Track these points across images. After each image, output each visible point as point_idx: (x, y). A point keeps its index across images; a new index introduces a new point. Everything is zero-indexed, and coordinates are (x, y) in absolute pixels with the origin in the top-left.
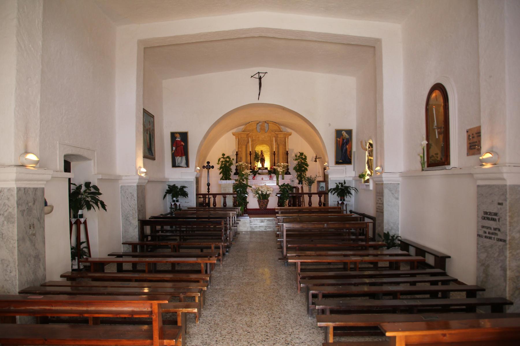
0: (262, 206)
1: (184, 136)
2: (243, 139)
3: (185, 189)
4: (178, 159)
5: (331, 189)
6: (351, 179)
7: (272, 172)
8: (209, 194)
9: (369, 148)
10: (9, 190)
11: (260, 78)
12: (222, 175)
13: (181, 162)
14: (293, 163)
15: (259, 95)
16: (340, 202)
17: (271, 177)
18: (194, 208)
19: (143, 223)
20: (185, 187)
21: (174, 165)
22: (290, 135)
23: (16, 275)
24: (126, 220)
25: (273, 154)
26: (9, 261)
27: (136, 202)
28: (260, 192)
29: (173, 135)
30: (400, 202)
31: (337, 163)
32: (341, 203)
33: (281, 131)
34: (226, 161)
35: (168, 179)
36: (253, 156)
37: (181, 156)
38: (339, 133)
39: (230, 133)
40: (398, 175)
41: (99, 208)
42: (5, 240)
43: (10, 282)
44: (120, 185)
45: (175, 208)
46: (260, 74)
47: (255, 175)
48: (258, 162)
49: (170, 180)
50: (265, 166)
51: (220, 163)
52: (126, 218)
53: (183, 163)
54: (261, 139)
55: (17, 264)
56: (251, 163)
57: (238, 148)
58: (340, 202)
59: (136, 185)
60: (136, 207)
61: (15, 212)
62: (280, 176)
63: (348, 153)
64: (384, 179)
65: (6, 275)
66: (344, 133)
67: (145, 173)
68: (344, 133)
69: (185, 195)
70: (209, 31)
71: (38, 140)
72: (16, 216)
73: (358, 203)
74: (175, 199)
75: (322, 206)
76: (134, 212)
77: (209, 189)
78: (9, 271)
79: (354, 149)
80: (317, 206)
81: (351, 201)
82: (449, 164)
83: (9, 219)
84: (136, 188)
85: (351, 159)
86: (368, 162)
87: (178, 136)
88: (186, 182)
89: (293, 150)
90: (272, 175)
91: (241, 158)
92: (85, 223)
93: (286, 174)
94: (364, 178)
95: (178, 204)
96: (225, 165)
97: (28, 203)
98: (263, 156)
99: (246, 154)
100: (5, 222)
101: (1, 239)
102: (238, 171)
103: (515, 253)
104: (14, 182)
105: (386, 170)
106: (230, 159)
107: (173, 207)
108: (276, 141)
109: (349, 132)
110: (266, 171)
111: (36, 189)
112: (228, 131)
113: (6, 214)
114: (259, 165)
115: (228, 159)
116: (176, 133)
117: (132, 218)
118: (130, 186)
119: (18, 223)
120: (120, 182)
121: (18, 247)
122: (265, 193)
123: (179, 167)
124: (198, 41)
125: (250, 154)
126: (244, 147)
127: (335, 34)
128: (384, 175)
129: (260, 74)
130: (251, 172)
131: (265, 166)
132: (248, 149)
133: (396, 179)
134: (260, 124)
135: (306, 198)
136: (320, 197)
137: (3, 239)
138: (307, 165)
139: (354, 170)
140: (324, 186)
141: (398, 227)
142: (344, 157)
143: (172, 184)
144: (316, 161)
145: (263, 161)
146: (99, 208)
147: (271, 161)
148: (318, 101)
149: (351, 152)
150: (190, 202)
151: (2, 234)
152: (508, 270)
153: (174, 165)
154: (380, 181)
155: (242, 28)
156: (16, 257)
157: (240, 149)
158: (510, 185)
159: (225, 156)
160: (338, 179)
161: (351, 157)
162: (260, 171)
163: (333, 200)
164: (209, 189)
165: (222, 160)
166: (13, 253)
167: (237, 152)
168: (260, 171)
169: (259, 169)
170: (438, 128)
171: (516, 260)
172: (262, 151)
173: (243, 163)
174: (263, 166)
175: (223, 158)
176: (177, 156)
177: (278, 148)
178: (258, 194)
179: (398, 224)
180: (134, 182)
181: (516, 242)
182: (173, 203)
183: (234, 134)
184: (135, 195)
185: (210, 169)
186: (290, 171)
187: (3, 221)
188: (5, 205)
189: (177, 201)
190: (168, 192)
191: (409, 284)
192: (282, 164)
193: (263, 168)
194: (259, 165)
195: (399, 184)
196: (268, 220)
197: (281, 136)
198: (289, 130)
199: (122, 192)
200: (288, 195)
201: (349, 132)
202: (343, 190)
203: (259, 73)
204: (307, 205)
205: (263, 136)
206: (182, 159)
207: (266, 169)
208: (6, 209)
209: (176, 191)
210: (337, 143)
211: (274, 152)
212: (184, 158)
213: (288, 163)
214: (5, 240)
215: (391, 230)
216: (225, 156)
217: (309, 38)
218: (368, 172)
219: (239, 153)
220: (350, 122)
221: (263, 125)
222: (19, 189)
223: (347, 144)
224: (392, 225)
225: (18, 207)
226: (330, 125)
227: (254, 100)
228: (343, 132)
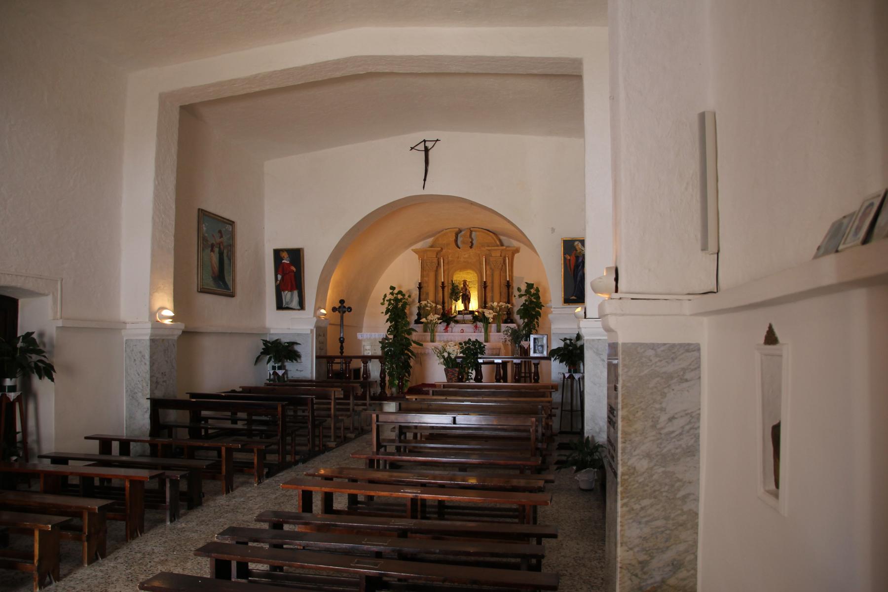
1: (296, 255)
2: (433, 262)
3: (297, 348)
4: (287, 295)
11: (427, 150)
13: (292, 301)
14: (518, 302)
15: (425, 180)
16: (567, 375)
18: (311, 381)
19: (157, 405)
20: (297, 344)
21: (280, 306)
22: (517, 251)
25: (484, 287)
28: (446, 355)
29: (277, 253)
32: (569, 377)
34: (396, 300)
35: (269, 329)
37: (291, 290)
49: (272, 332)
51: (387, 303)
52: (132, 396)
53: (295, 303)
54: (462, 260)
56: (443, 303)
57: (422, 276)
59: (148, 338)
62: (493, 327)
70: (271, 69)
76: (145, 384)
77: (342, 348)
84: (148, 343)
87: (285, 255)
88: (299, 335)
91: (427, 294)
93: (506, 322)
96: (395, 307)
99: (436, 287)
103: (637, 507)
106: (404, 295)
112: (407, 248)
114: (460, 306)
115: (400, 297)
118: (140, 340)
120: (123, 332)
122: (453, 357)
125: (443, 287)
126: (432, 274)
127: (493, 58)
129: (428, 144)
130: (439, 319)
145: (466, 299)
152: (619, 545)
153: (280, 306)
155: (325, 59)
157: (426, 279)
158: (624, 344)
162: (460, 317)
164: (342, 348)
165: (389, 297)
167: (420, 284)
168: (460, 317)
169: (460, 312)
171: (640, 523)
172: (465, 282)
173: (429, 303)
174: (466, 307)
175: (392, 294)
176: (284, 290)
178: (443, 357)
181: (641, 479)
183: (416, 251)
184: (147, 357)
185: (344, 312)
190: (266, 352)
194: (460, 306)
203: (425, 141)
205: (466, 254)
206: (292, 295)
207: (472, 312)
209: (281, 351)
211: (485, 282)
212: (296, 293)
215: (599, 433)
216: (396, 291)
217: (453, 69)
219: (424, 285)
221: (463, 237)
226: (553, 230)
228: (576, 243)
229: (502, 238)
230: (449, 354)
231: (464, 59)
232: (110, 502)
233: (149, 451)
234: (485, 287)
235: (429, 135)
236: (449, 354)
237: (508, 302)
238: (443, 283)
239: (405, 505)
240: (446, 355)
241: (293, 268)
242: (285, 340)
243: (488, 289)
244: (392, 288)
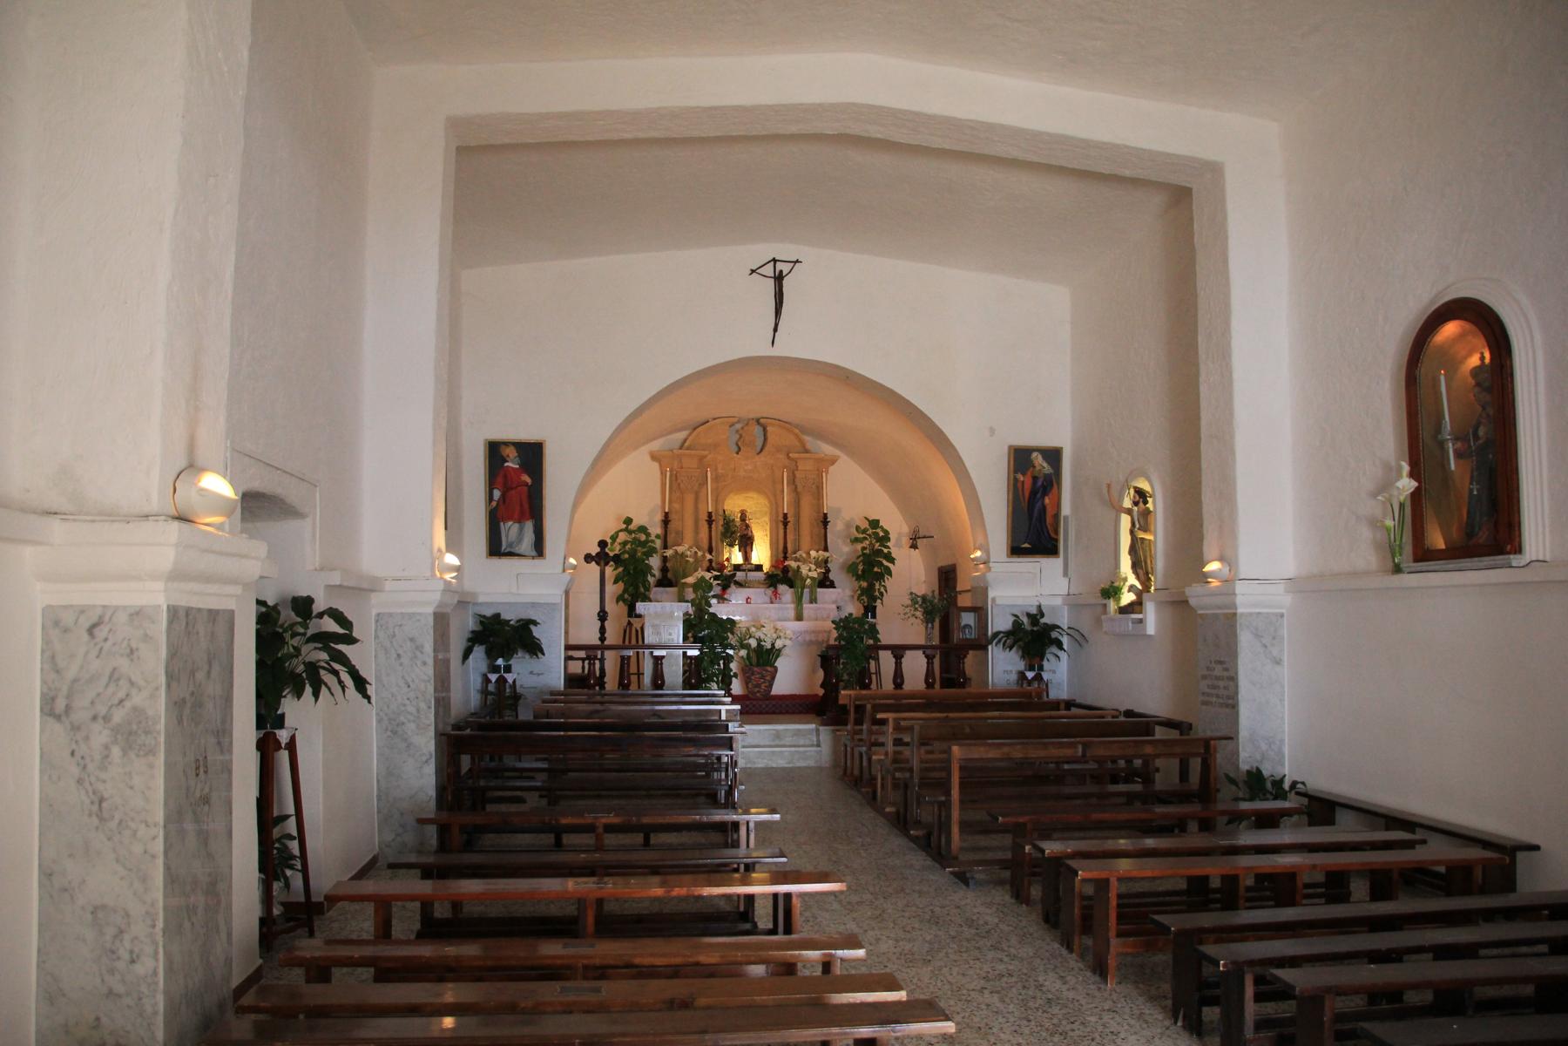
0: (758, 686)
1: (532, 454)
2: (683, 472)
4: (510, 530)
5: (996, 635)
6: (1058, 601)
7: (780, 577)
8: (603, 648)
9: (1136, 504)
10: (137, 614)
11: (779, 278)
12: (621, 586)
13: (520, 539)
14: (841, 551)
15: (775, 330)
17: (775, 593)
18: (560, 693)
20: (535, 623)
22: (833, 461)
23: (155, 973)
24: (394, 733)
25: (783, 524)
26: (128, 915)
27: (430, 671)
28: (753, 643)
29: (495, 450)
30: (1285, 672)
31: (1016, 551)
33: (807, 451)
35: (474, 595)
36: (718, 527)
37: (520, 520)
38: (1020, 458)
39: (644, 451)
40: (1281, 588)
41: (343, 688)
42: (113, 824)
43: (128, 1001)
44: (374, 612)
45: (501, 698)
46: (780, 266)
47: (725, 588)
48: (732, 545)
49: (481, 599)
50: (755, 560)
53: (527, 543)
54: (742, 473)
55: (160, 924)
58: (1030, 675)
59: (430, 610)
60: (431, 689)
61: (159, 709)
63: (1049, 520)
64: (1239, 600)
65: (112, 971)
66: (1038, 459)
67: (458, 569)
68: (1038, 459)
69: (535, 648)
71: (222, 419)
72: (161, 726)
73: (1129, 673)
74: (500, 662)
75: (937, 686)
76: (423, 705)
77: (602, 630)
78: (127, 956)
79: (1066, 509)
80: (922, 686)
81: (1059, 674)
82: (1518, 550)
83: (130, 736)
84: (431, 620)
85: (1057, 540)
86: (1133, 550)
87: (511, 452)
88: (534, 605)
89: (839, 511)
90: (782, 588)
91: (680, 534)
92: (291, 746)
94: (1119, 600)
95: (510, 678)
96: (633, 554)
97: (193, 673)
98: (748, 526)
100: (116, 751)
101: (95, 821)
102: (669, 575)
104: (160, 585)
105: (1245, 570)
106: (648, 535)
107: (491, 688)
108: (793, 481)
109: (1053, 456)
110: (759, 575)
111: (213, 614)
112: (636, 448)
113: (118, 716)
114: (737, 557)
115: (643, 538)
116: (506, 444)
117: (412, 726)
118: (411, 616)
119: (168, 752)
120: (375, 598)
121: (166, 853)
123: (511, 554)
124: (641, 135)
125: (710, 521)
126: (689, 499)
128: (1240, 588)
129: (780, 266)
131: (755, 560)
132: (702, 507)
133: (1279, 599)
134: (738, 426)
135: (887, 659)
136: (930, 658)
137: (102, 819)
138: (892, 561)
139: (1065, 574)
140: (972, 623)
141: (1280, 753)
142: (1035, 533)
143: (489, 612)
144: (914, 546)
145: (746, 543)
146: (343, 688)
147: (773, 545)
148: (975, 355)
149: (1057, 516)
150: (547, 672)
151: (102, 800)
154: (1226, 607)
156: (159, 895)
157: (676, 506)
159: (631, 527)
160: (1020, 602)
161: (1057, 532)
162: (740, 576)
163: (1003, 667)
166: (144, 879)
169: (737, 568)
170: (1456, 439)
174: (747, 557)
176: (505, 520)
177: (797, 503)
178: (747, 647)
179: (1282, 741)
180: (426, 601)
182: (493, 677)
183: (654, 457)
186: (831, 576)
187: (107, 747)
188: (114, 676)
189: (508, 669)
190: (475, 639)
191: (418, 872)
192: (813, 553)
193: (748, 566)
194: (737, 557)
195: (1282, 616)
196: (798, 733)
197: (806, 466)
198: (827, 449)
199: (381, 634)
200: (845, 655)
201: (1053, 456)
202: (1034, 637)
203: (775, 261)
204: (888, 685)
205: (747, 464)
206: (521, 530)
207: (759, 568)
208: (121, 694)
209: (504, 636)
210: (1015, 488)
212: (529, 526)
213: (826, 549)
214: (113, 824)
218: (1132, 580)
219: (672, 517)
220: (1052, 426)
221: (755, 433)
222: (173, 612)
223: (1045, 493)
224: (1264, 747)
225: (168, 686)
226: (992, 431)
227: (762, 349)
228: (1035, 455)
229: (807, 438)
230: (759, 640)
231: (1035, 137)
232: (1156, 917)
233: (434, 842)
234: (785, 524)
235: (785, 251)
236: (759, 640)
237: (826, 549)
238: (710, 514)
239: (1248, 900)
240: (753, 643)
241: (527, 479)
242: (510, 616)
243: (790, 526)
244: (628, 521)
